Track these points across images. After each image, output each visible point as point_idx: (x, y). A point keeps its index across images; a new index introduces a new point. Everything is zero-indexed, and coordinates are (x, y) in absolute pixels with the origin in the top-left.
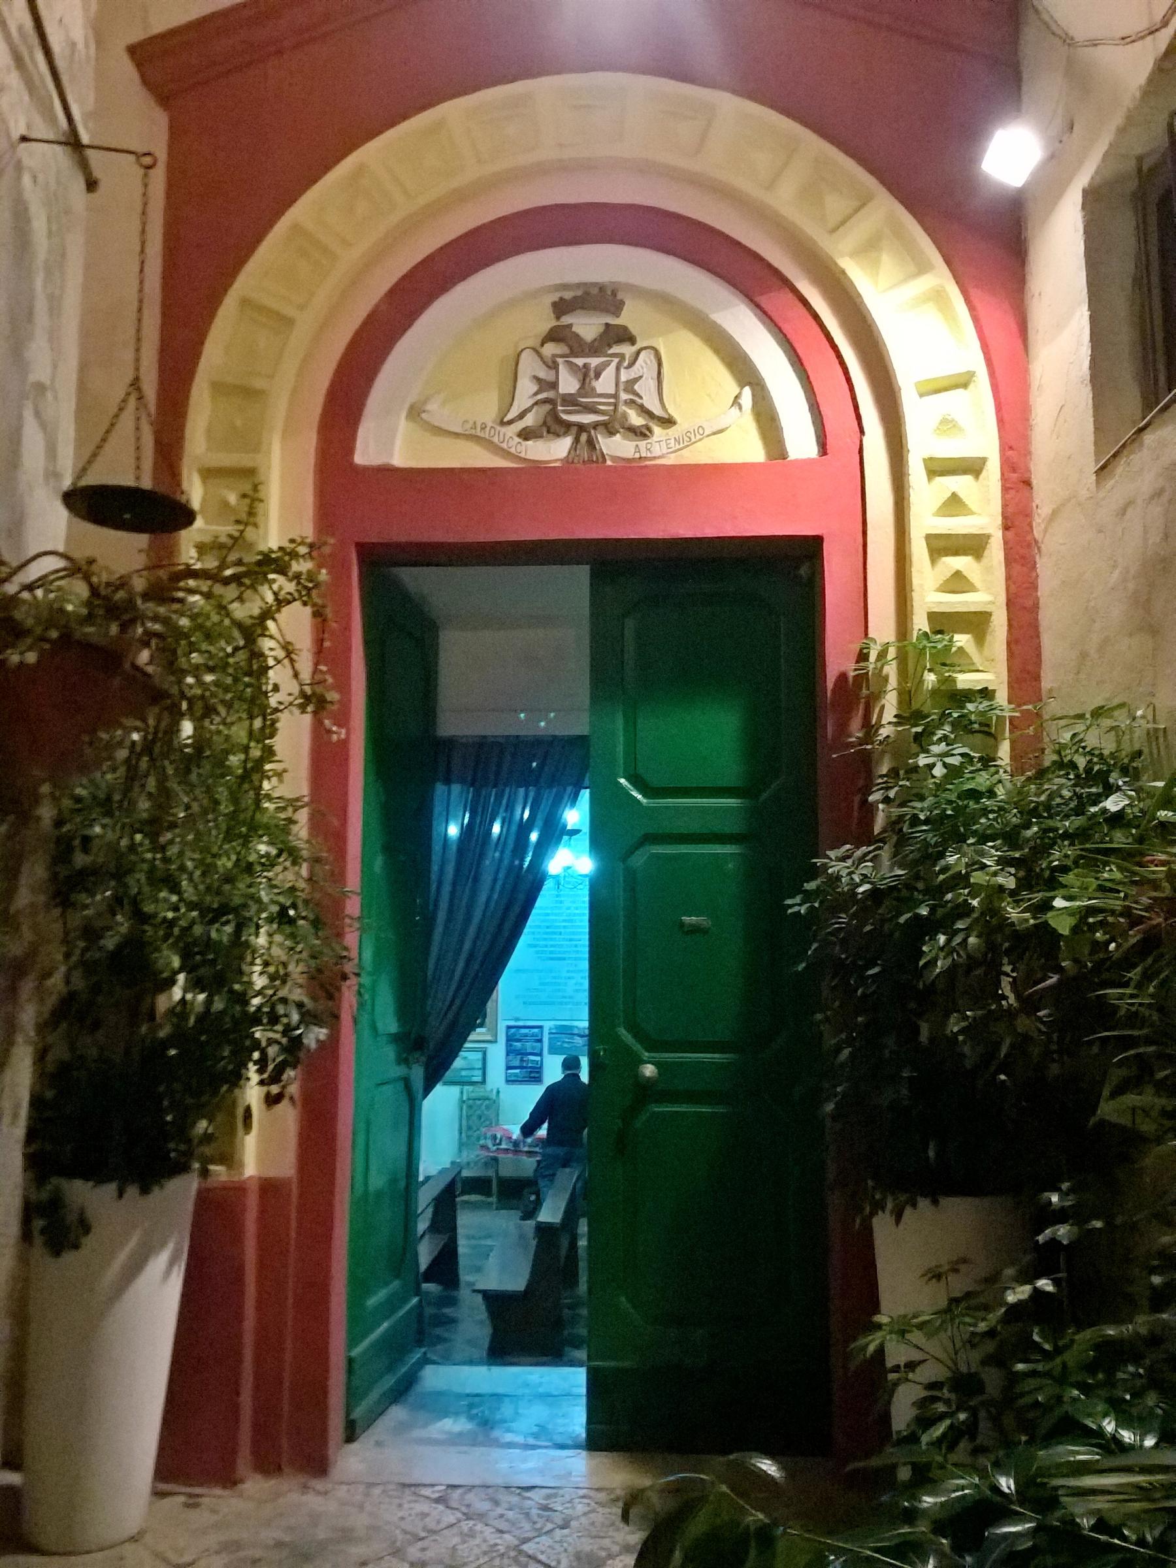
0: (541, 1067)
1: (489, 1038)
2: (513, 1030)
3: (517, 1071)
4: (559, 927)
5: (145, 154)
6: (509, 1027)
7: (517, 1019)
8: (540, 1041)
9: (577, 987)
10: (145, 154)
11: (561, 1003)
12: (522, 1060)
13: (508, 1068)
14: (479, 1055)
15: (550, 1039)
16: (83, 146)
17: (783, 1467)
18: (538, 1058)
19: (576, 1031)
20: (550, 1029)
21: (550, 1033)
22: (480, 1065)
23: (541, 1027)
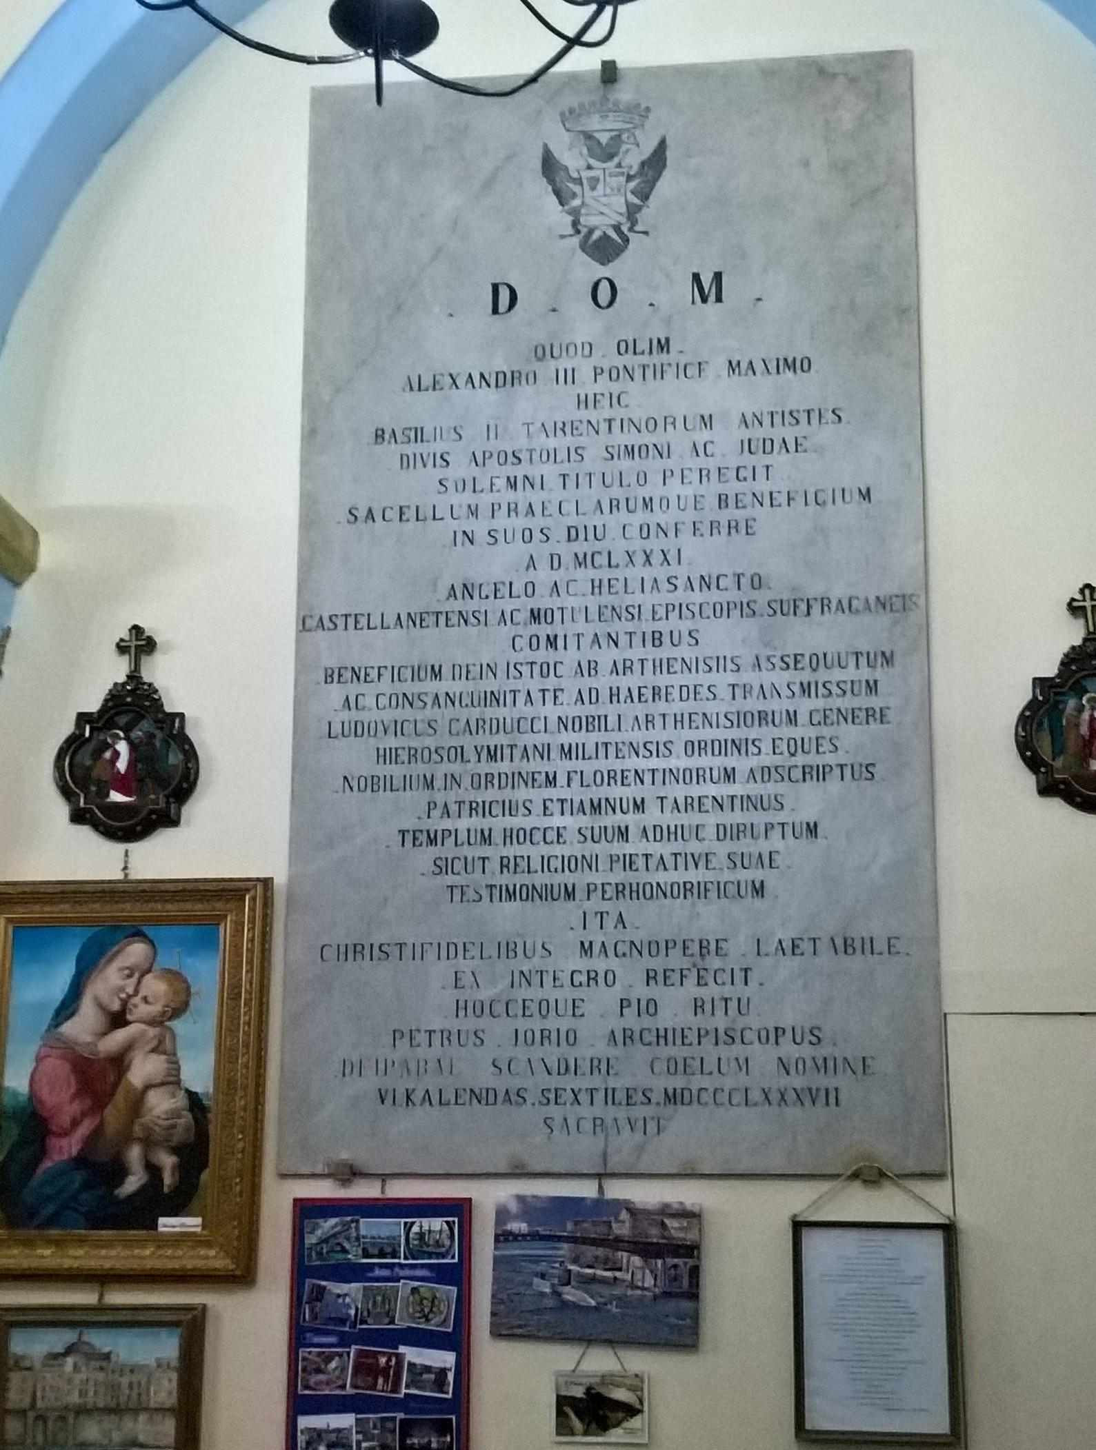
0: (461, 1403)
1: (214, 1259)
2: (329, 1225)
3: (345, 1421)
4: (544, 752)
5: (304, 623)
6: (306, 1211)
7: (349, 1173)
8: (458, 1275)
9: (631, 1020)
10: (304, 623)
11: (553, 1097)
12: (367, 1368)
13: (299, 1404)
14: (167, 1347)
15: (497, 1261)
16: (574, 1371)
17: (131, 1197)
18: (445, 1359)
19: (623, 1228)
20: (502, 1215)
21: (503, 1237)
22: (165, 1390)
23: (460, 1209)
